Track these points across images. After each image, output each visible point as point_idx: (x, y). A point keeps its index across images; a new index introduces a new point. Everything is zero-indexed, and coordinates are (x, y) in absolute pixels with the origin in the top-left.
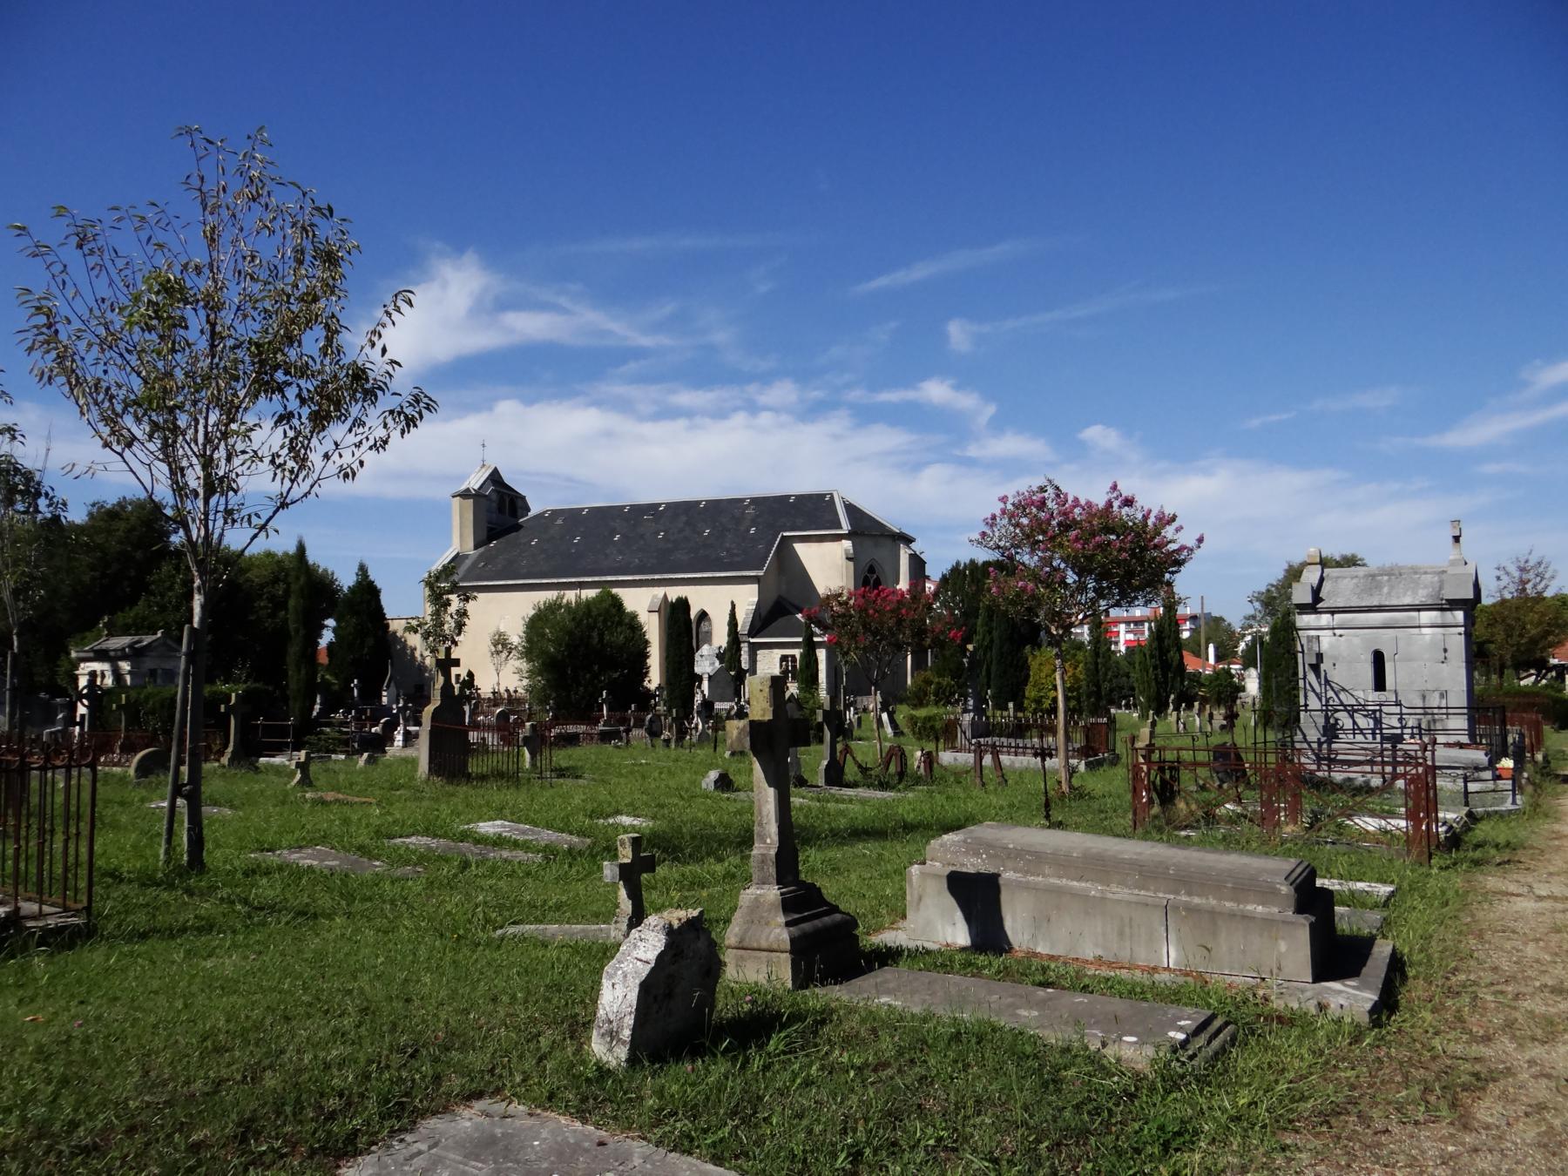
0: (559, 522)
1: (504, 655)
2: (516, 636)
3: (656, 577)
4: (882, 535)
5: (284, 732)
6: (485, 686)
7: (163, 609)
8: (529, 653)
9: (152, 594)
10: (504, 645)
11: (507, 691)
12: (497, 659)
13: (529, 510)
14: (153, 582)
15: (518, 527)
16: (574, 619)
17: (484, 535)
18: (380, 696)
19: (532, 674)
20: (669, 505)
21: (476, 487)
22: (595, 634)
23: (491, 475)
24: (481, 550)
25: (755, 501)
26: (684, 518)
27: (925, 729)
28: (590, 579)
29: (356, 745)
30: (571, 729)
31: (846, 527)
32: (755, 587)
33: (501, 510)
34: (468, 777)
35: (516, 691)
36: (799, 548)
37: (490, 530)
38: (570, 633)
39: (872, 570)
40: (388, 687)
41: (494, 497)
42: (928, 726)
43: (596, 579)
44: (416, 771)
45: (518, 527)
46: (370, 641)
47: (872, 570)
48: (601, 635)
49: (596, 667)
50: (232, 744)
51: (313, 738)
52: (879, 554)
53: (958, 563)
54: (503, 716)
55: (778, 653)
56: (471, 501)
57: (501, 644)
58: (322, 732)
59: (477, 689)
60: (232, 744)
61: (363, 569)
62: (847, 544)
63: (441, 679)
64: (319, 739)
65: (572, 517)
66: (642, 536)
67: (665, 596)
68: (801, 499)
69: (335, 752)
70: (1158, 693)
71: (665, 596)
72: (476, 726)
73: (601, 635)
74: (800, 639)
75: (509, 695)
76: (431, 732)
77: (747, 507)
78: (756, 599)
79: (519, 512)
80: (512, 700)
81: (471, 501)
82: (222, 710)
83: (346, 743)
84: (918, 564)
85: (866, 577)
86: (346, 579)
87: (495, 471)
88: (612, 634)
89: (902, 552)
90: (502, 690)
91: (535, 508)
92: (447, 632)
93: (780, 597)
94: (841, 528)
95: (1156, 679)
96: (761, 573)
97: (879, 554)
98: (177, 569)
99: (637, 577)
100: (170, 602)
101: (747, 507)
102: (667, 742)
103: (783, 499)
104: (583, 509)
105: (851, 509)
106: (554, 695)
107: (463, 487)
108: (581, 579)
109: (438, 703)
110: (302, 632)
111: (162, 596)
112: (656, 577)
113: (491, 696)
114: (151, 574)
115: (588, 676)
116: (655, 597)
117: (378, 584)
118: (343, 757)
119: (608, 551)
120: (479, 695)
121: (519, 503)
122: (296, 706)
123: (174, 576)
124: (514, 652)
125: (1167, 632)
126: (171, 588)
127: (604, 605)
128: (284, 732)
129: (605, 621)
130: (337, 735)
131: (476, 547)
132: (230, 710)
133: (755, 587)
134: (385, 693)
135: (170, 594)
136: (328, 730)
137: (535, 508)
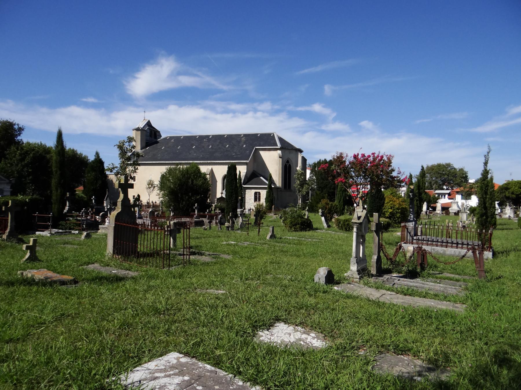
0: (172, 141)
1: (152, 189)
2: (157, 182)
3: (209, 162)
4: (292, 149)
5: (48, 219)
6: (144, 200)
7: (12, 165)
8: (161, 188)
9: (7, 158)
10: (152, 185)
11: (152, 202)
12: (149, 190)
13: (161, 136)
14: (8, 154)
15: (157, 142)
16: (182, 174)
17: (144, 145)
18: (103, 203)
19: (164, 196)
20: (213, 136)
21: (142, 127)
22: (190, 181)
23: (147, 123)
24: (143, 150)
25: (245, 135)
26: (219, 141)
27: (344, 225)
28: (184, 162)
29: (84, 226)
30: (183, 220)
31: (279, 146)
32: (246, 166)
33: (151, 136)
34: (139, 255)
35: (156, 202)
36: (262, 153)
37: (147, 143)
38: (180, 180)
39: (288, 162)
40: (106, 199)
41: (148, 131)
42: (346, 223)
43: (186, 162)
44: (105, 251)
45: (157, 142)
46: (100, 182)
47: (288, 162)
48: (192, 181)
49: (190, 194)
50: (9, 228)
51: (63, 223)
52: (291, 156)
53: (320, 160)
54: (152, 213)
55: (254, 191)
56: (140, 132)
57: (151, 184)
58: (68, 220)
59: (141, 201)
60: (9, 228)
61: (97, 154)
62: (279, 152)
63: (122, 196)
64: (66, 223)
65: (177, 139)
66: (203, 147)
67: (212, 169)
68: (262, 135)
69: (73, 229)
70: (418, 210)
71: (212, 169)
72: (140, 217)
73: (192, 181)
74: (267, 186)
75: (153, 204)
76: (115, 228)
77: (242, 137)
78: (246, 171)
79: (158, 137)
80: (155, 206)
81: (140, 132)
82: (3, 209)
83: (79, 225)
84: (304, 160)
85: (286, 164)
86: (91, 158)
87: (149, 121)
88: (197, 181)
89: (299, 155)
90: (151, 202)
91: (163, 136)
92: (128, 172)
93: (254, 170)
94: (277, 146)
95: (417, 205)
96: (248, 161)
97: (291, 156)
98: (18, 149)
99: (202, 162)
100: (14, 162)
101: (242, 137)
102: (228, 227)
103: (256, 135)
104: (181, 137)
105: (281, 139)
106: (173, 205)
107: (137, 127)
108: (181, 162)
109: (120, 210)
110: (59, 172)
111: (11, 159)
112: (209, 162)
113: (146, 204)
114: (6, 150)
115: (187, 197)
116: (208, 169)
117: (103, 160)
118: (77, 232)
119: (191, 152)
120: (142, 203)
121: (158, 134)
122: (55, 207)
123: (16, 152)
124: (156, 188)
125: (421, 186)
126: (14, 157)
127: (193, 169)
128: (48, 219)
129: (194, 176)
130: (75, 221)
131: (141, 149)
132: (8, 210)
133: (246, 166)
134: (105, 202)
135: (14, 159)
136: (71, 219)
137: (163, 136)
